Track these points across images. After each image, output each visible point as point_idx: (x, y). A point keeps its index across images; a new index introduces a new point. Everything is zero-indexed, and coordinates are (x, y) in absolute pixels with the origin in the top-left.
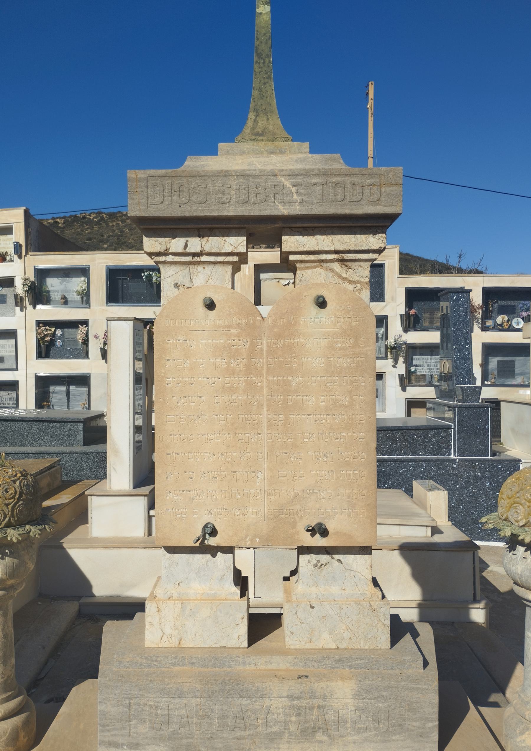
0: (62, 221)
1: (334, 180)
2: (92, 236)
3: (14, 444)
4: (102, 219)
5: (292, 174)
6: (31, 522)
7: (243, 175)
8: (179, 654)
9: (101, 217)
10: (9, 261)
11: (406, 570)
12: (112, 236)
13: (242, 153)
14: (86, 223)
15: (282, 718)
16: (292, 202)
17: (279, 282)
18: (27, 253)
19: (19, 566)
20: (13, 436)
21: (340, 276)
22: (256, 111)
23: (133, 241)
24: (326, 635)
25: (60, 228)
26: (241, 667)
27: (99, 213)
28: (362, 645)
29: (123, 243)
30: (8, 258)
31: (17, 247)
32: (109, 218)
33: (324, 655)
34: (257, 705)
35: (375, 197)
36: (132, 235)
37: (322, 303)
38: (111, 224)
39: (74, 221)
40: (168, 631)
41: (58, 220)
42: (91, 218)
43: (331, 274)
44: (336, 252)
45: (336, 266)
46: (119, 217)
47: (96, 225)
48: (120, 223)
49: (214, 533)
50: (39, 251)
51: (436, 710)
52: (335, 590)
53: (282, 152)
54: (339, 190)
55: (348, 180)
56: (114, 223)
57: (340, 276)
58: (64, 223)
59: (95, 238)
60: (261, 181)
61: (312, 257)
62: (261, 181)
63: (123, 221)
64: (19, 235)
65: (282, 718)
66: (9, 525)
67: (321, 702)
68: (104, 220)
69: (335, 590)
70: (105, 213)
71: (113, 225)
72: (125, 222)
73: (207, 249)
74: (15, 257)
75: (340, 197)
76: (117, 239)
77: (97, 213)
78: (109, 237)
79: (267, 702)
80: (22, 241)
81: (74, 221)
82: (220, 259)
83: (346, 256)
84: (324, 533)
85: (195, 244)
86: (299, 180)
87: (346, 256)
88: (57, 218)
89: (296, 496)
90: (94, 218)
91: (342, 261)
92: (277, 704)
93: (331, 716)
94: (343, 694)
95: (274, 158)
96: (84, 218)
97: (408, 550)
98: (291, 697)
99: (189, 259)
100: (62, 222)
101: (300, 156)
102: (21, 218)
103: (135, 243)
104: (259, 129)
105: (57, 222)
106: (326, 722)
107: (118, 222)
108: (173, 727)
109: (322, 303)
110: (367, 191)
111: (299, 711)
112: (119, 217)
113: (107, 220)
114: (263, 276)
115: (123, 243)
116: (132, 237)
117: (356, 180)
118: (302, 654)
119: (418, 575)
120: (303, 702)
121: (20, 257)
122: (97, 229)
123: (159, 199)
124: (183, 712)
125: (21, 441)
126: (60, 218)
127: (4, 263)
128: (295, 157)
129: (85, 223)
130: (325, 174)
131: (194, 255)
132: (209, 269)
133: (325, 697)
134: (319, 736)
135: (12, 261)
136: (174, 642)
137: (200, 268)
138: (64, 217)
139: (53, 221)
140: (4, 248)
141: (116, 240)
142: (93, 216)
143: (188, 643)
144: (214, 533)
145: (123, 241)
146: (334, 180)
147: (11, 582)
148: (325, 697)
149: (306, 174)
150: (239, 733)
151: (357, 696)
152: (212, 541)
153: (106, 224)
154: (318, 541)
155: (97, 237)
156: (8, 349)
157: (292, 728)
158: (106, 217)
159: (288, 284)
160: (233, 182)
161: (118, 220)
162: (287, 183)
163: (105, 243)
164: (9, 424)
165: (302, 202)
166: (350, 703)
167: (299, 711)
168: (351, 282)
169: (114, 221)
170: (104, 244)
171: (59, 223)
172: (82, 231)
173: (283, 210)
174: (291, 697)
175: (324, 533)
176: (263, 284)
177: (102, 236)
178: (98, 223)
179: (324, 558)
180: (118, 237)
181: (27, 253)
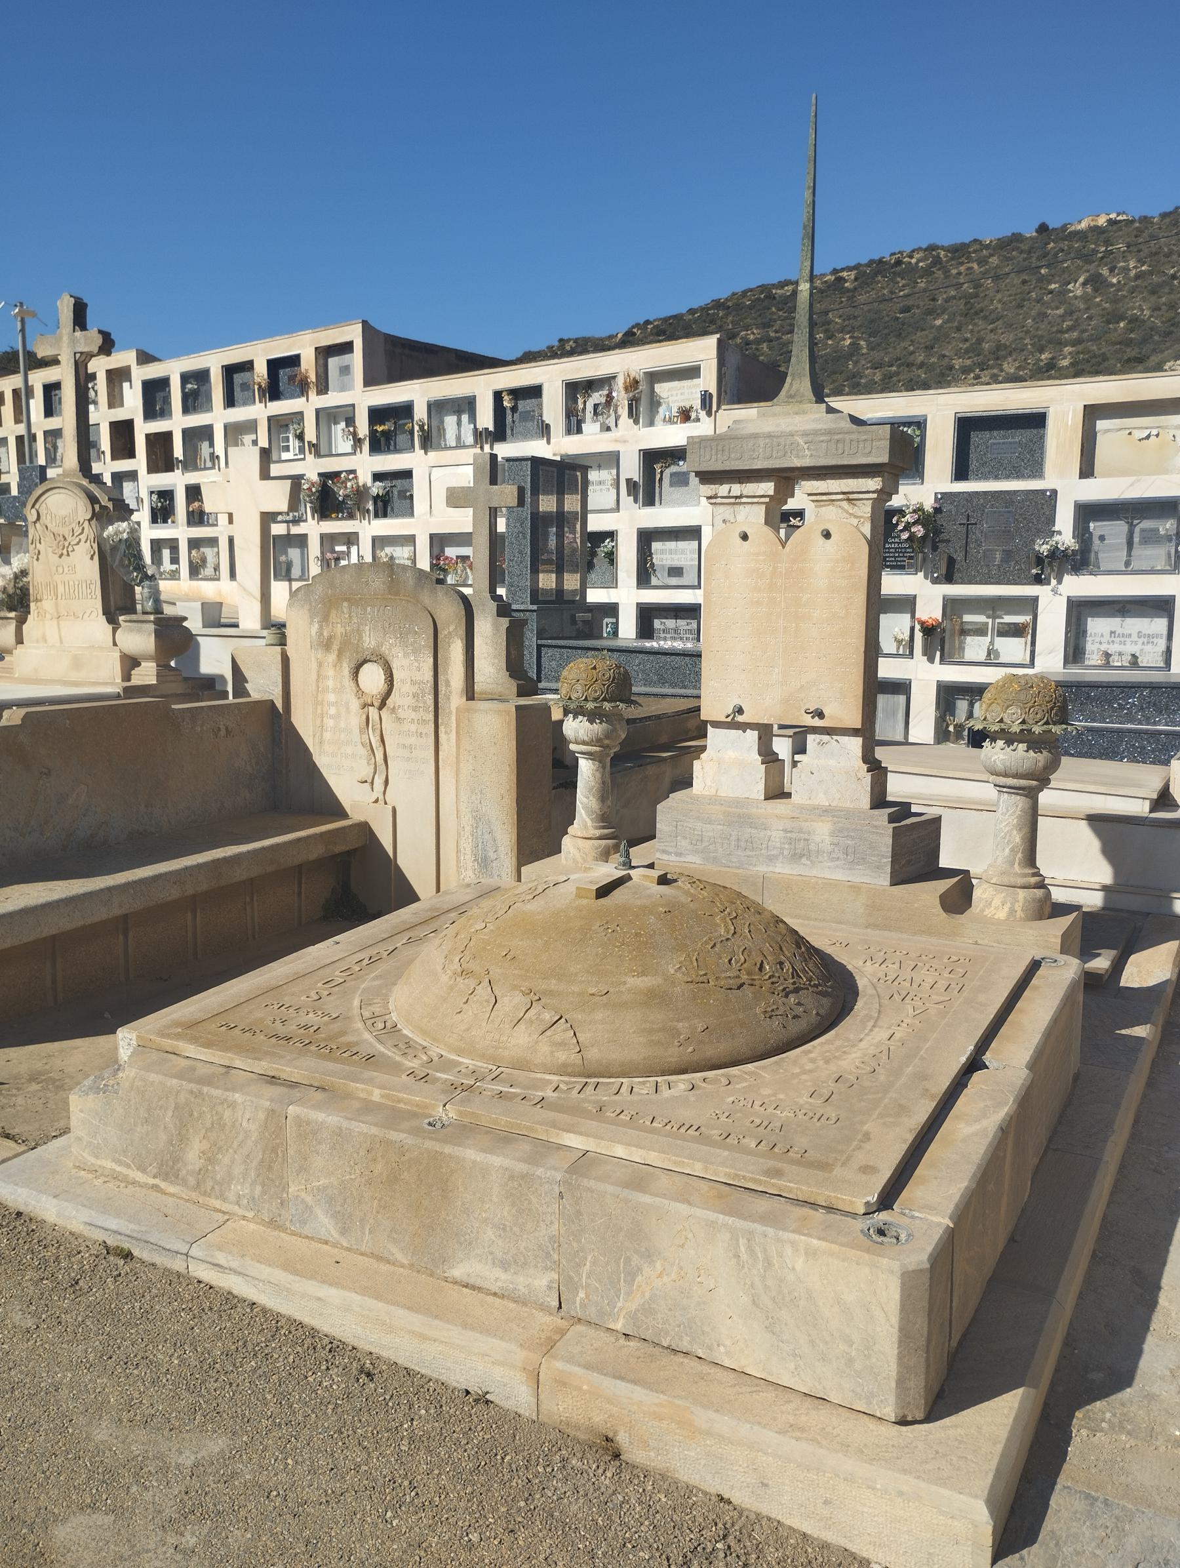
0: (853, 275)
1: (836, 437)
2: (911, 303)
3: (673, 685)
4: (937, 261)
5: (805, 434)
6: (621, 701)
7: (769, 436)
8: (714, 800)
9: (933, 257)
10: (694, 421)
11: (1095, 844)
12: (954, 297)
13: (775, 415)
14: (902, 275)
15: (778, 845)
16: (804, 456)
17: (1130, 434)
18: (719, 408)
19: (613, 731)
20: (672, 674)
21: (847, 512)
22: (793, 375)
23: (999, 306)
24: (821, 795)
25: (848, 290)
26: (754, 810)
27: (932, 248)
28: (848, 805)
29: (976, 313)
30: (693, 415)
31: (706, 398)
32: (952, 259)
33: (814, 809)
34: (762, 834)
35: (867, 450)
36: (998, 292)
37: (827, 535)
38: (954, 272)
39: (876, 273)
40: (709, 783)
41: (845, 274)
42: (914, 261)
43: (840, 511)
44: (844, 493)
45: (845, 504)
46: (975, 251)
47: (921, 277)
48: (975, 266)
49: (740, 711)
50: (739, 402)
51: (890, 849)
52: (832, 762)
53: (804, 412)
54: (840, 446)
55: (847, 437)
56: (962, 269)
57: (847, 512)
58: (856, 279)
59: (918, 307)
60: (782, 440)
61: (824, 498)
62: (782, 440)
63: (982, 262)
64: (708, 380)
65: (778, 845)
66: (604, 700)
67: (806, 836)
68: (941, 263)
69: (832, 762)
70: (943, 248)
71: (960, 274)
72: (987, 263)
73: (745, 493)
74: (703, 414)
75: (840, 451)
76: (966, 304)
77: (926, 250)
78: (947, 301)
79: (769, 833)
80: (713, 390)
81: (876, 273)
82: (755, 500)
83: (851, 496)
84: (820, 714)
85: (736, 489)
86: (810, 438)
87: (851, 496)
88: (843, 270)
89: (802, 687)
90: (919, 261)
91: (848, 500)
92: (776, 835)
93: (812, 847)
94: (822, 832)
95: (798, 419)
96: (899, 262)
97: (1097, 821)
98: (785, 831)
99: (733, 500)
100: (853, 277)
101: (817, 416)
102: (713, 353)
103: (1003, 310)
104: (792, 392)
105: (841, 280)
106: (809, 851)
107: (970, 265)
108: (705, 844)
109: (827, 535)
110: (861, 445)
111: (791, 841)
112: (975, 251)
113: (947, 262)
114: (1101, 425)
115: (976, 313)
116: (999, 296)
117: (854, 436)
118: (802, 808)
119: (1110, 852)
120: (793, 835)
121: (709, 414)
122: (923, 285)
123: (708, 457)
124: (711, 834)
125: (682, 682)
126: (849, 269)
127: (687, 424)
128: (813, 417)
129: (899, 275)
130: (829, 432)
131: (736, 497)
132: (748, 507)
133: (809, 833)
134: (804, 860)
135: (698, 420)
136: (713, 792)
137: (742, 507)
138: (857, 267)
139: (833, 278)
140: (688, 400)
141: (962, 307)
142: (917, 256)
143: (722, 794)
144: (740, 711)
145: (978, 307)
146: (836, 437)
147: (606, 742)
148: (809, 833)
149: (816, 433)
150: (748, 853)
151: (832, 834)
152: (740, 718)
153: (945, 273)
154: (817, 722)
155: (922, 304)
156: (689, 556)
157: (786, 852)
158: (946, 256)
159: (1148, 437)
160: (761, 442)
161: (970, 260)
162: (801, 441)
163: (938, 316)
164: (668, 659)
165: (811, 456)
166: (828, 840)
167: (791, 841)
168: (856, 517)
169: (962, 263)
170: (935, 319)
171: (846, 281)
172: (892, 292)
173: (797, 463)
174: (785, 831)
175: (820, 714)
176: (1101, 440)
177: (934, 300)
178: (927, 272)
179: (826, 738)
180: (968, 298)
181: (719, 408)
